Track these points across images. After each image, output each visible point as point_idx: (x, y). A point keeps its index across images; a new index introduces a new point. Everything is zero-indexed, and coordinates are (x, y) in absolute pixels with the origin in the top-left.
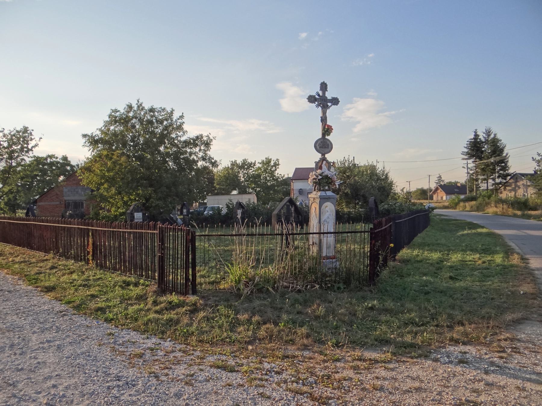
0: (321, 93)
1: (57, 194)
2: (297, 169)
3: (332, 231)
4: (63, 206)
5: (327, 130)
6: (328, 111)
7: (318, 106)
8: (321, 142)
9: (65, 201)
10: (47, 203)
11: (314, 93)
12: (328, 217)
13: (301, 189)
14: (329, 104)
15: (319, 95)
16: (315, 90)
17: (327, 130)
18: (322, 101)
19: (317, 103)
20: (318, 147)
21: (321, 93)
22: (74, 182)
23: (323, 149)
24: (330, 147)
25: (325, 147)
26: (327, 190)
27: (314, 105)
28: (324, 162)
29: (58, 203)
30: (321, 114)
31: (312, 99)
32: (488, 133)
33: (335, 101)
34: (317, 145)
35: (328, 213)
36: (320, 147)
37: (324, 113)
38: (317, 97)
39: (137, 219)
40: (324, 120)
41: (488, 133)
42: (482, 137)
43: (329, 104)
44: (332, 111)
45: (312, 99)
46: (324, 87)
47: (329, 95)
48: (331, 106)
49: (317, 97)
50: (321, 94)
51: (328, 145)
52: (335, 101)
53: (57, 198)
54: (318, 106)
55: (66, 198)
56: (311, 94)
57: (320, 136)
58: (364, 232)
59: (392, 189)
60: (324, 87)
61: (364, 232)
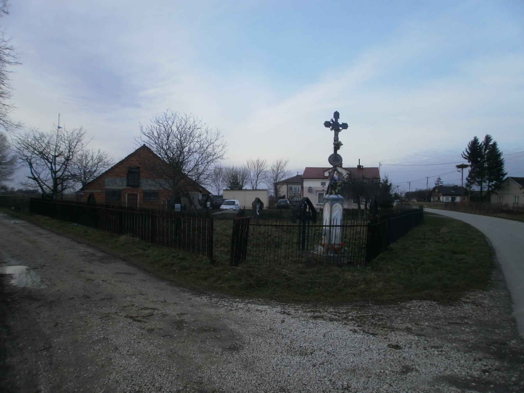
2: (307, 169)
3: (340, 224)
5: (337, 145)
6: (340, 133)
7: (332, 129)
9: (106, 190)
11: (329, 120)
12: (337, 215)
13: (310, 187)
14: (341, 128)
15: (333, 121)
16: (330, 117)
17: (337, 145)
18: (335, 125)
20: (331, 161)
27: (329, 129)
28: (336, 172)
29: (100, 191)
31: (327, 124)
32: (488, 139)
33: (345, 126)
35: (337, 211)
37: (336, 135)
38: (331, 122)
40: (336, 139)
41: (488, 139)
42: (481, 140)
43: (341, 128)
44: (343, 135)
45: (327, 124)
46: (337, 115)
47: (340, 121)
49: (331, 122)
52: (345, 126)
57: (332, 152)
60: (337, 115)
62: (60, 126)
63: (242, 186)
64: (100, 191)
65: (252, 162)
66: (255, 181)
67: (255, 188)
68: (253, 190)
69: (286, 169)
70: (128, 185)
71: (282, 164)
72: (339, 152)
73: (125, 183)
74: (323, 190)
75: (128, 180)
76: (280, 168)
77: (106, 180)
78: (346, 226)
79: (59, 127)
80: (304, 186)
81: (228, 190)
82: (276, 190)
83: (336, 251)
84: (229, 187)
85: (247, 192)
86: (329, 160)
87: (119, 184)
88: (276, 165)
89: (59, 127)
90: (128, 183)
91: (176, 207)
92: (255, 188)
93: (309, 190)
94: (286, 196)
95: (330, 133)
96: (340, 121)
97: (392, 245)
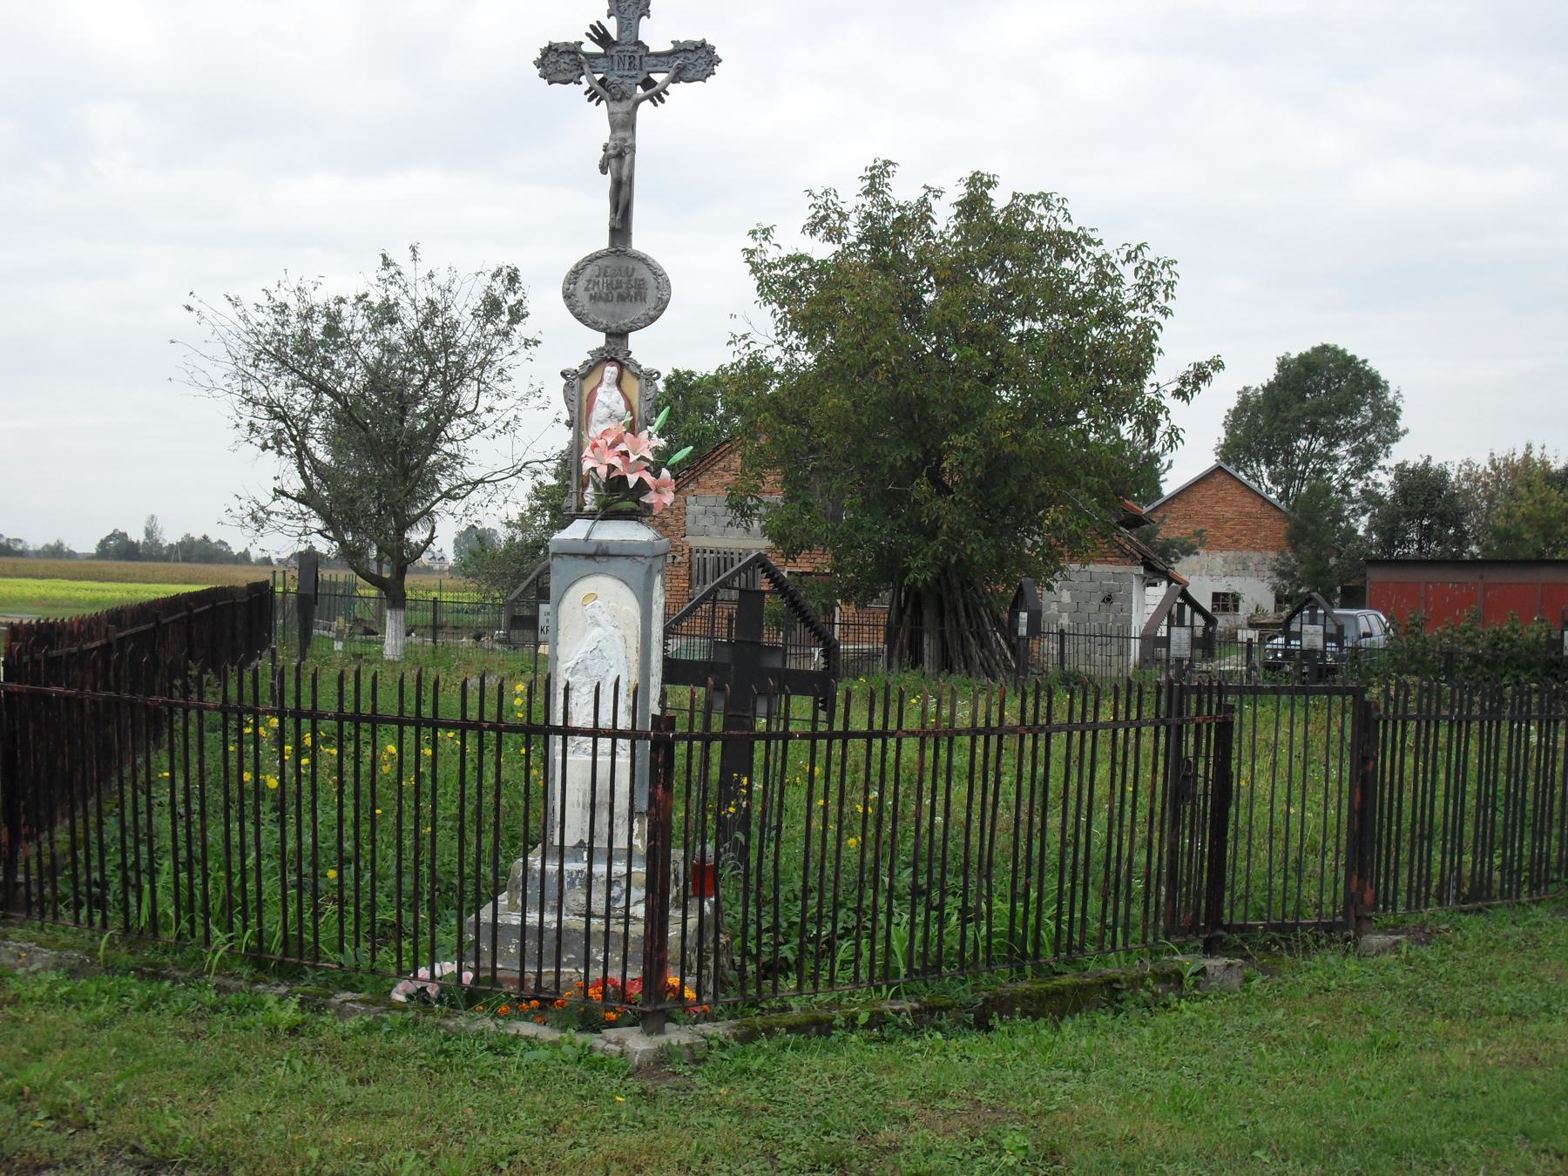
7: (593, 95)
15: (600, 35)
18: (619, 68)
20: (582, 296)
23: (609, 307)
24: (651, 294)
25: (622, 298)
27: (576, 92)
31: (559, 63)
33: (694, 61)
34: (582, 283)
37: (624, 125)
38: (591, 47)
49: (591, 47)
52: (694, 61)
55: (694, 542)
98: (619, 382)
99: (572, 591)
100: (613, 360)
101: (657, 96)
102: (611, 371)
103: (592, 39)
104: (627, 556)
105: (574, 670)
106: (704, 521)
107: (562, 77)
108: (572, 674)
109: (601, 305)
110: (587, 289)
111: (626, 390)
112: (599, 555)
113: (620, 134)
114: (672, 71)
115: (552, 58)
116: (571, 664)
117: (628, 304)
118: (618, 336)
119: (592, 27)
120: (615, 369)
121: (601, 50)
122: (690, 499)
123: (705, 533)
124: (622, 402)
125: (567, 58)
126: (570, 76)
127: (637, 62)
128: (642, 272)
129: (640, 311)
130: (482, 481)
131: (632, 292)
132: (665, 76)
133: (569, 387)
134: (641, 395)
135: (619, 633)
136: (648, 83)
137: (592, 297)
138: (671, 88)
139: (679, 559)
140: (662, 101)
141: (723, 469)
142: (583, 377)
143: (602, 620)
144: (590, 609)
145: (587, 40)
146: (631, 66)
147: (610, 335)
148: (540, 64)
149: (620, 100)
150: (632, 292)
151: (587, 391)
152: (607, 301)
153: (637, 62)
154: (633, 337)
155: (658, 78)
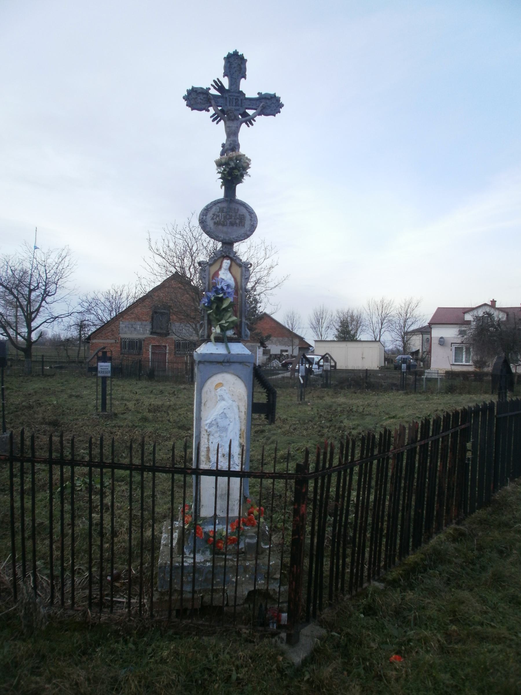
0: (226, 83)
1: (113, 331)
2: (439, 309)
4: (119, 345)
5: (233, 169)
7: (216, 118)
8: (222, 210)
10: (101, 341)
12: (224, 415)
13: (442, 338)
15: (220, 87)
16: (210, 74)
17: (233, 169)
18: (230, 102)
19: (212, 111)
20: (210, 223)
21: (226, 83)
22: (133, 316)
23: (225, 229)
24: (248, 223)
25: (232, 224)
26: (231, 340)
27: (205, 116)
29: (113, 341)
30: (223, 138)
31: (197, 99)
33: (270, 105)
34: (210, 215)
35: (222, 404)
36: (216, 224)
37: (232, 134)
38: (213, 92)
39: (102, 372)
44: (255, 138)
45: (197, 99)
46: (235, 64)
47: (250, 88)
48: (255, 115)
49: (213, 92)
50: (226, 86)
51: (242, 219)
52: (270, 105)
53: (113, 335)
54: (216, 118)
55: (122, 336)
56: (197, 85)
58: (229, 474)
59: (50, 339)
60: (235, 64)
61: (229, 474)
62: (38, 246)
63: (354, 336)
64: (113, 341)
65: (375, 302)
66: (378, 330)
67: (378, 340)
68: (376, 341)
69: (416, 313)
70: (152, 333)
71: (413, 305)
72: (242, 192)
73: (148, 328)
74: (462, 343)
75: (152, 325)
76: (409, 310)
77: (122, 325)
78: (172, 470)
79: (36, 248)
80: (432, 336)
81: (334, 341)
82: (405, 343)
83: (214, 544)
84: (336, 337)
85: (365, 345)
86: (203, 222)
87: (139, 331)
88: (403, 305)
89: (36, 248)
90: (152, 328)
91: (99, 369)
92: (378, 340)
93: (440, 341)
94: (421, 351)
95: (209, 133)
96: (250, 88)
97: (509, 488)
98: (230, 269)
99: (209, 382)
100: (228, 257)
101: (249, 121)
102: (226, 263)
103: (215, 88)
104: (240, 363)
105: (211, 425)
106: (125, 330)
107: (199, 106)
108: (209, 427)
109: (220, 227)
110: (212, 219)
111: (234, 272)
112: (224, 363)
113: (232, 138)
114: (259, 109)
115: (194, 95)
116: (208, 421)
117: (235, 227)
118: (228, 244)
119: (214, 81)
120: (229, 261)
121: (219, 94)
122: (121, 322)
123: (125, 333)
124: (233, 279)
125: (202, 96)
126: (204, 106)
127: (240, 102)
128: (243, 211)
129: (242, 231)
130: (57, 317)
131: (238, 221)
132: (254, 111)
133: (203, 270)
134: (242, 276)
135: (235, 404)
136: (245, 115)
137: (215, 223)
138: (257, 118)
139: (117, 341)
140: (252, 125)
141: (131, 313)
142: (211, 265)
143: (226, 397)
144: (219, 391)
145: (212, 88)
146: (237, 105)
147: (224, 243)
148: (236, 53)
149: (233, 120)
150: (238, 221)
151: (212, 273)
152: (223, 225)
153: (240, 102)
154: (235, 245)
155: (251, 112)
